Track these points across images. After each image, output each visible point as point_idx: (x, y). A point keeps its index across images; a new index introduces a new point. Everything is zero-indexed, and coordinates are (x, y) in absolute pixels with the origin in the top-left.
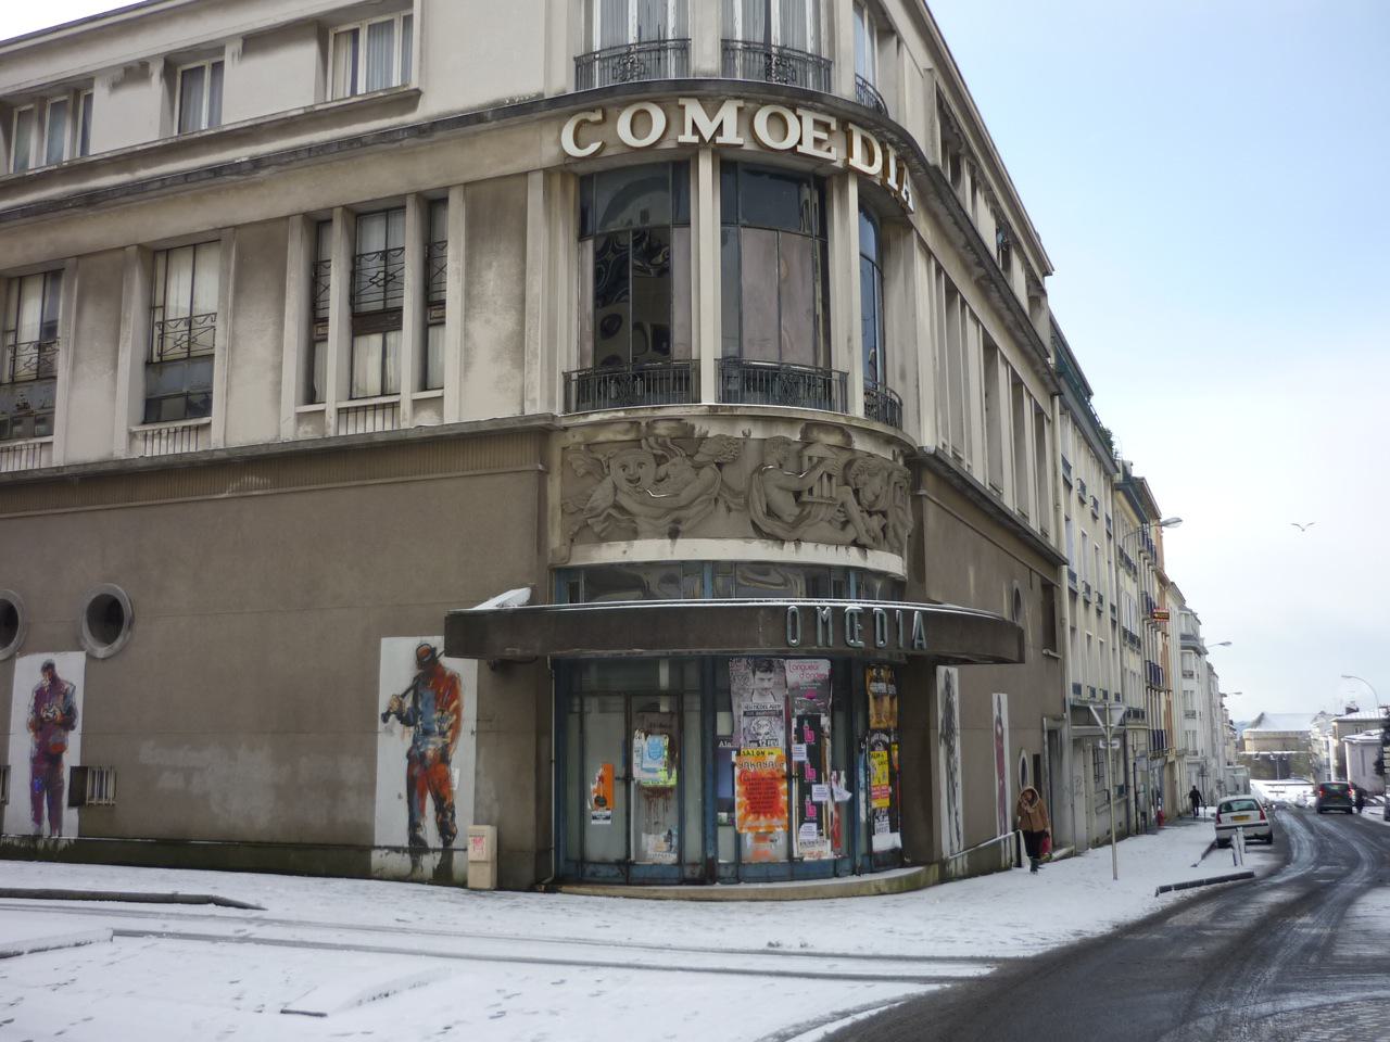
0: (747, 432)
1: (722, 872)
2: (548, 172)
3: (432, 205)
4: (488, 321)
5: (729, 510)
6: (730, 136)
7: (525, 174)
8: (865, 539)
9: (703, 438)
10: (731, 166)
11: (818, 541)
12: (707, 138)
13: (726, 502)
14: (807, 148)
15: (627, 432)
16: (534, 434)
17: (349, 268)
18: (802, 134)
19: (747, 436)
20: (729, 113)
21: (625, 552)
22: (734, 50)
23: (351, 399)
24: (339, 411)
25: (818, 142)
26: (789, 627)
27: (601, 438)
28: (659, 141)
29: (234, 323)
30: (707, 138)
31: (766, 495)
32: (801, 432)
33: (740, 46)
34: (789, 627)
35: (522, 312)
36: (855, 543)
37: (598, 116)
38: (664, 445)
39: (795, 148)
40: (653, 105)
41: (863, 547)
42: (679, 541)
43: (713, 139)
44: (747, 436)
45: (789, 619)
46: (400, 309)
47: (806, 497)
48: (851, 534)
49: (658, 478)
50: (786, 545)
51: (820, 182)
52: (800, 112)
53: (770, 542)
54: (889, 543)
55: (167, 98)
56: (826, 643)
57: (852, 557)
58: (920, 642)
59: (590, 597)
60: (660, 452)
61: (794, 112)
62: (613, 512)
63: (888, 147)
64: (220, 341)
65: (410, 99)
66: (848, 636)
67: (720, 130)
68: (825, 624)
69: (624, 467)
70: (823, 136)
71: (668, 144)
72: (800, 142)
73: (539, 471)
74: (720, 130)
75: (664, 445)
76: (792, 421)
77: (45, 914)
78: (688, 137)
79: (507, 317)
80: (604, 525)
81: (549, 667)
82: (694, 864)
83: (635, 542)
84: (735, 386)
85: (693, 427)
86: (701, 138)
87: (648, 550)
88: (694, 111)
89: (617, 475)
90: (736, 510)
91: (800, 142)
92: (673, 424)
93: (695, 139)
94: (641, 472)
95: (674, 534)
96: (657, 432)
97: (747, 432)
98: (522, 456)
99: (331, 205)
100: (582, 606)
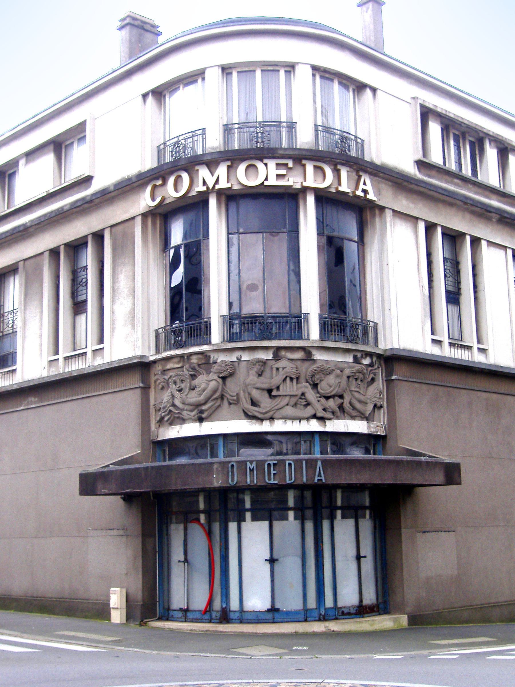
0: (239, 357)
1: (232, 616)
2: (144, 215)
3: (99, 237)
4: (121, 304)
5: (230, 404)
6: (223, 184)
7: (133, 218)
8: (320, 414)
9: (215, 363)
10: (230, 198)
11: (285, 418)
12: (211, 187)
13: (228, 399)
14: (272, 181)
15: (179, 362)
16: (141, 367)
17: (71, 277)
18: (268, 174)
19: (239, 359)
20: (222, 170)
21: (178, 432)
22: (233, 129)
23: (74, 350)
24: (94, 351)
25: (279, 176)
26: (266, 474)
27: (169, 366)
28: (188, 192)
29: (25, 313)
30: (211, 187)
31: (249, 394)
32: (273, 354)
33: (236, 126)
34: (230, 474)
35: (134, 297)
36: (314, 417)
37: (159, 182)
38: (194, 369)
39: (263, 183)
40: (183, 172)
41: (322, 419)
42: (204, 424)
43: (214, 186)
44: (239, 359)
45: (230, 469)
46: (85, 301)
47: (274, 393)
48: (309, 411)
49: (192, 388)
50: (264, 422)
51: (292, 197)
52: (265, 161)
53: (254, 421)
54: (347, 414)
55: (288, 64)
56: (252, 480)
57: (314, 426)
58: (319, 478)
59: (171, 458)
60: (192, 373)
61: (262, 161)
62: (171, 408)
63: (339, 167)
64: (19, 323)
65: (87, 180)
66: (267, 478)
67: (217, 182)
68: (252, 470)
69: (175, 383)
70: (283, 172)
71: (193, 193)
72: (266, 179)
73: (141, 387)
74: (217, 182)
75: (194, 369)
76: (267, 348)
77: (213, 660)
78: (201, 188)
79: (129, 300)
80: (169, 416)
81: (152, 498)
82: (218, 611)
83: (183, 425)
84: (236, 329)
85: (210, 357)
86: (208, 188)
87: (190, 429)
88: (203, 172)
89: (173, 388)
90: (234, 404)
91: (266, 179)
92: (200, 356)
93: (204, 189)
94: (183, 386)
95: (201, 420)
96: (192, 361)
97: (239, 357)
98: (135, 381)
99: (59, 245)
100: (167, 463)
